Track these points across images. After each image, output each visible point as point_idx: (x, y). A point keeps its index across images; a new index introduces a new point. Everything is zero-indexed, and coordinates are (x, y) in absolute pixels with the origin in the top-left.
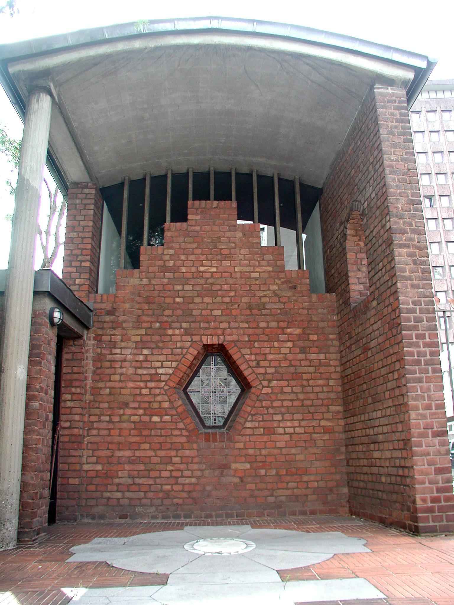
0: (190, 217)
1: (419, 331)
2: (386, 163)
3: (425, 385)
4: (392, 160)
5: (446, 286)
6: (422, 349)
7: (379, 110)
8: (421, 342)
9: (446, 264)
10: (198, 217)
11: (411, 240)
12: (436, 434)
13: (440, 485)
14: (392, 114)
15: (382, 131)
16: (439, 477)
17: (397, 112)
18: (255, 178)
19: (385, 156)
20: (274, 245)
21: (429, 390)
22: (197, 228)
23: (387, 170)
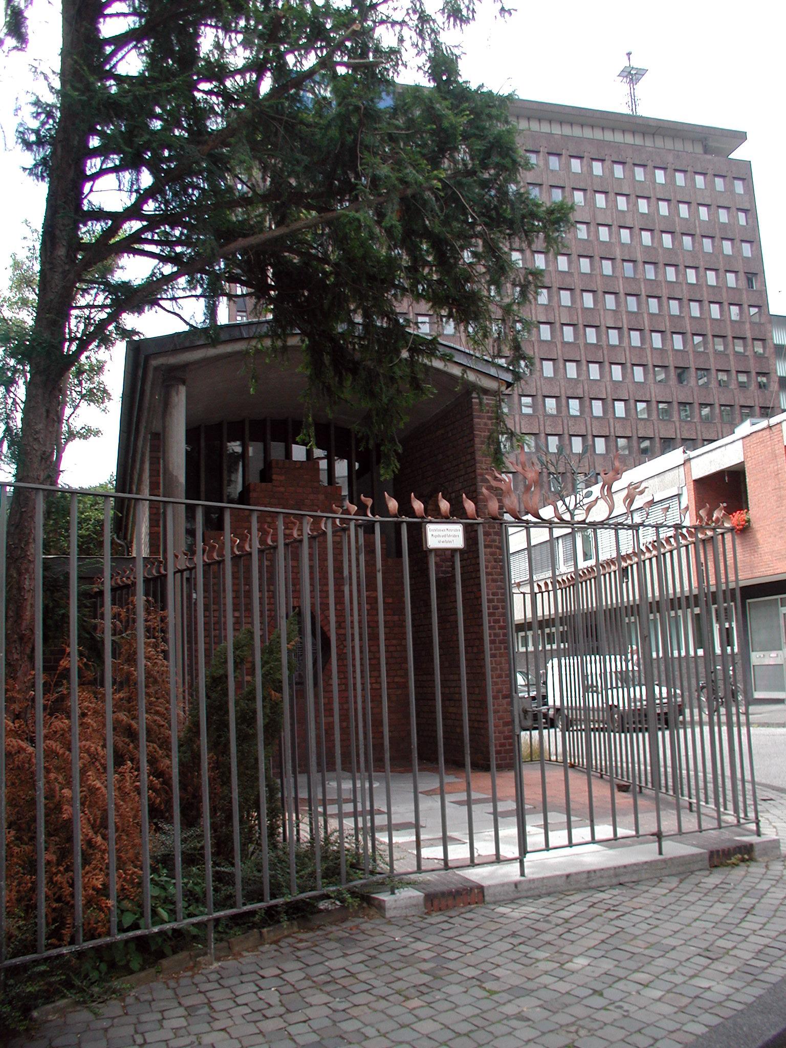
0: (274, 477)
1: (159, 496)
2: (479, 471)
3: (498, 659)
4: (482, 469)
5: (626, 392)
6: (497, 631)
7: (476, 420)
8: (497, 625)
9: (566, 432)
10: (282, 478)
11: (494, 541)
12: (505, 697)
13: (506, 733)
14: (486, 424)
15: (477, 440)
16: (506, 728)
17: (489, 422)
18: (333, 429)
19: (478, 465)
20: (283, 458)
21: (501, 663)
22: (282, 489)
23: (479, 478)
